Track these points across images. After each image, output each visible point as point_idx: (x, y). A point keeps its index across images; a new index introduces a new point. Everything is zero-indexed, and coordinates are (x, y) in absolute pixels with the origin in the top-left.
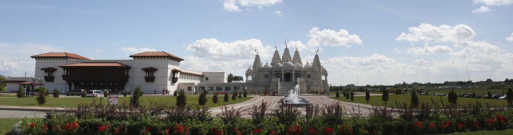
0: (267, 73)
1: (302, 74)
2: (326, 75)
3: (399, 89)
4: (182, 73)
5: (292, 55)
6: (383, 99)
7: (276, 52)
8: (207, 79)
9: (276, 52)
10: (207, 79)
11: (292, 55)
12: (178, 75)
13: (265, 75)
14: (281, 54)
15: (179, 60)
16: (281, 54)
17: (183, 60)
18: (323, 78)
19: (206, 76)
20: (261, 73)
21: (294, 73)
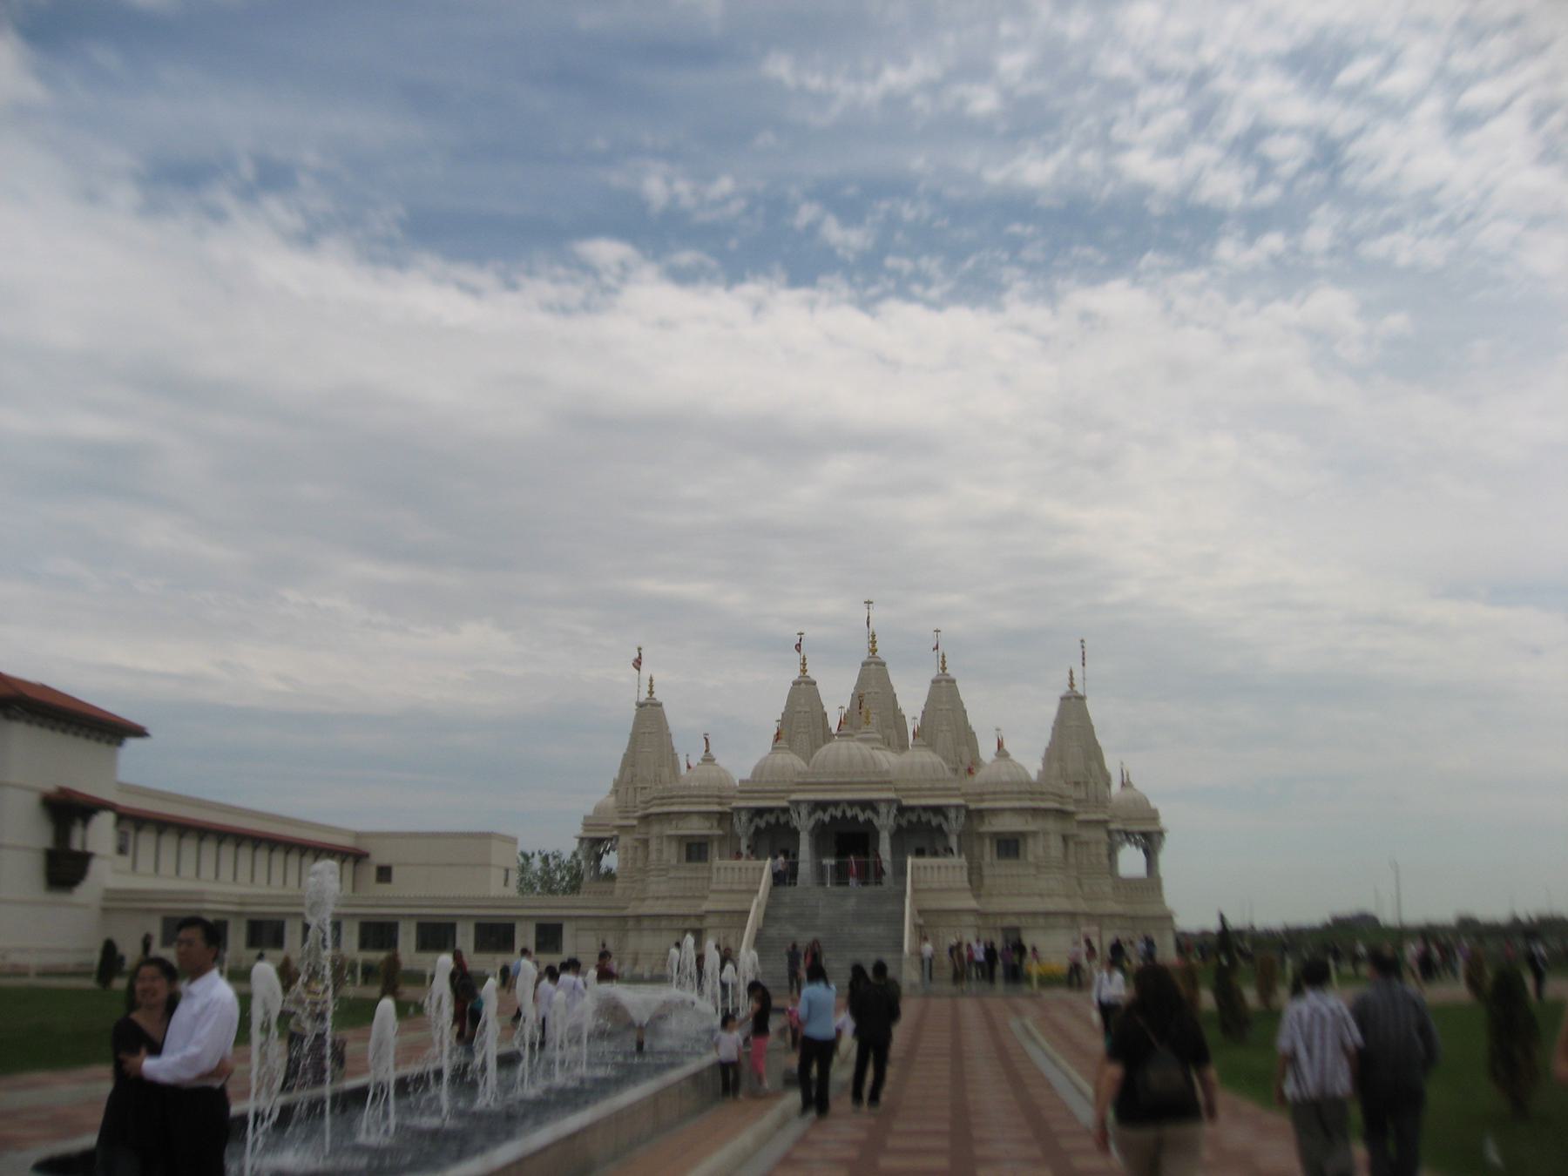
0: (696, 828)
1: (954, 825)
2: (1150, 842)
3: (1439, 947)
4: (134, 822)
5: (912, 699)
6: (107, 891)
7: (804, 688)
8: (384, 874)
9: (804, 688)
10: (384, 874)
11: (912, 699)
12: (100, 835)
13: (681, 839)
14: (836, 694)
15: (111, 730)
16: (836, 694)
17: (139, 732)
18: (1131, 861)
19: (379, 857)
20: (656, 829)
21: (885, 823)
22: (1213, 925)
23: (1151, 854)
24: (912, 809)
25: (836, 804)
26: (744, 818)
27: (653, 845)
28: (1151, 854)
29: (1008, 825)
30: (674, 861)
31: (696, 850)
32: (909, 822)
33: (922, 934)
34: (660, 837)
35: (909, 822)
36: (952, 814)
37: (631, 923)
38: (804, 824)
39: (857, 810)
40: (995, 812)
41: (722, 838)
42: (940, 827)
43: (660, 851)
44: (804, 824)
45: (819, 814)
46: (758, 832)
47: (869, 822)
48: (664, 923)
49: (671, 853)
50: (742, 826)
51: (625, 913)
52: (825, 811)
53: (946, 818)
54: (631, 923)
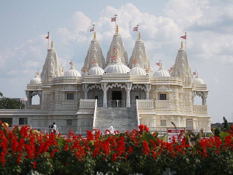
0: (70, 89)
1: (148, 90)
20: (57, 89)
22: (222, 122)
23: (203, 98)
24: (136, 85)
25: (114, 83)
26: (86, 87)
27: (57, 94)
28: (203, 98)
29: (163, 90)
30: (64, 99)
31: (70, 96)
32: (93, 88)
33: (140, 116)
34: (59, 92)
35: (93, 88)
36: (147, 86)
37: (49, 118)
38: (105, 90)
39: (140, 87)
40: (160, 86)
41: (78, 92)
42: (143, 90)
43: (59, 96)
44: (105, 90)
45: (109, 86)
46: (90, 90)
47: (124, 88)
48: (61, 118)
49: (63, 97)
50: (86, 90)
51: (48, 115)
52: (111, 85)
53: (145, 88)
54: (49, 118)
